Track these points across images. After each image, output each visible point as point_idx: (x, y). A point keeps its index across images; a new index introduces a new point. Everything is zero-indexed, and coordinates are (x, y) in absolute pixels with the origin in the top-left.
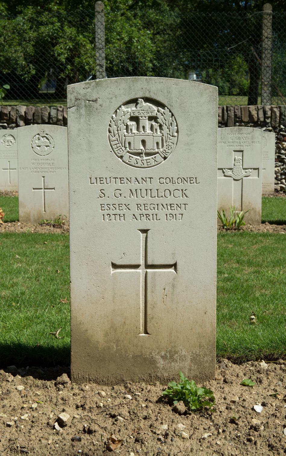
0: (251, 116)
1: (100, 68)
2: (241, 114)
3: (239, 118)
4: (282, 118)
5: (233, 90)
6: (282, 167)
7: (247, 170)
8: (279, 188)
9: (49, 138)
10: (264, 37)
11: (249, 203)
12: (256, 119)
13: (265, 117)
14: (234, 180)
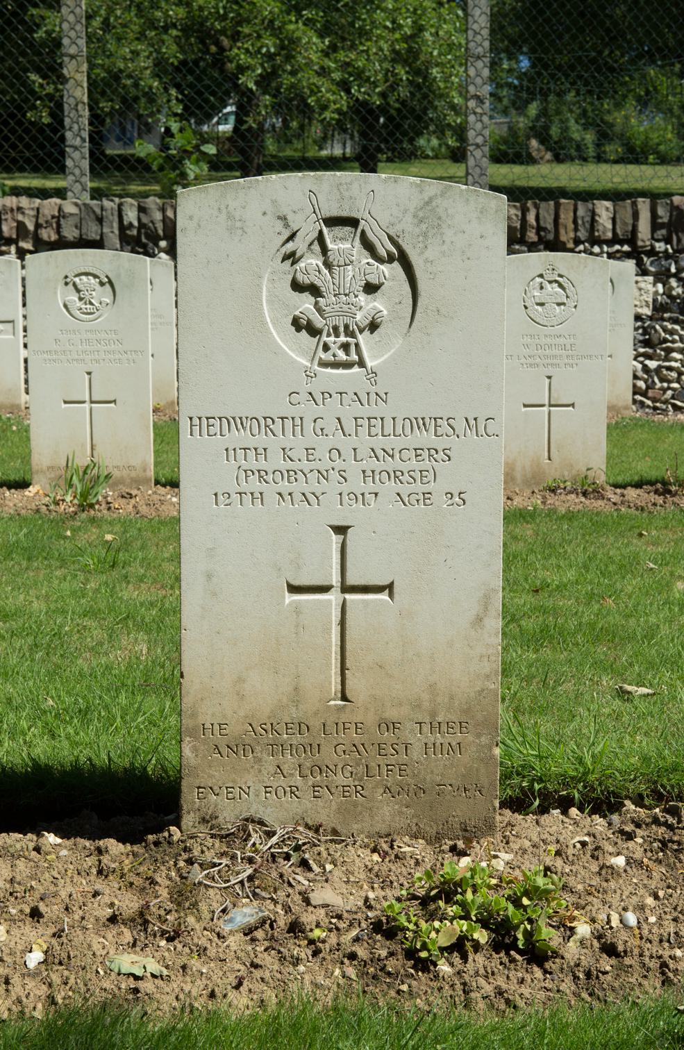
1: (477, 106)
5: (608, 148)
9: (565, 285)
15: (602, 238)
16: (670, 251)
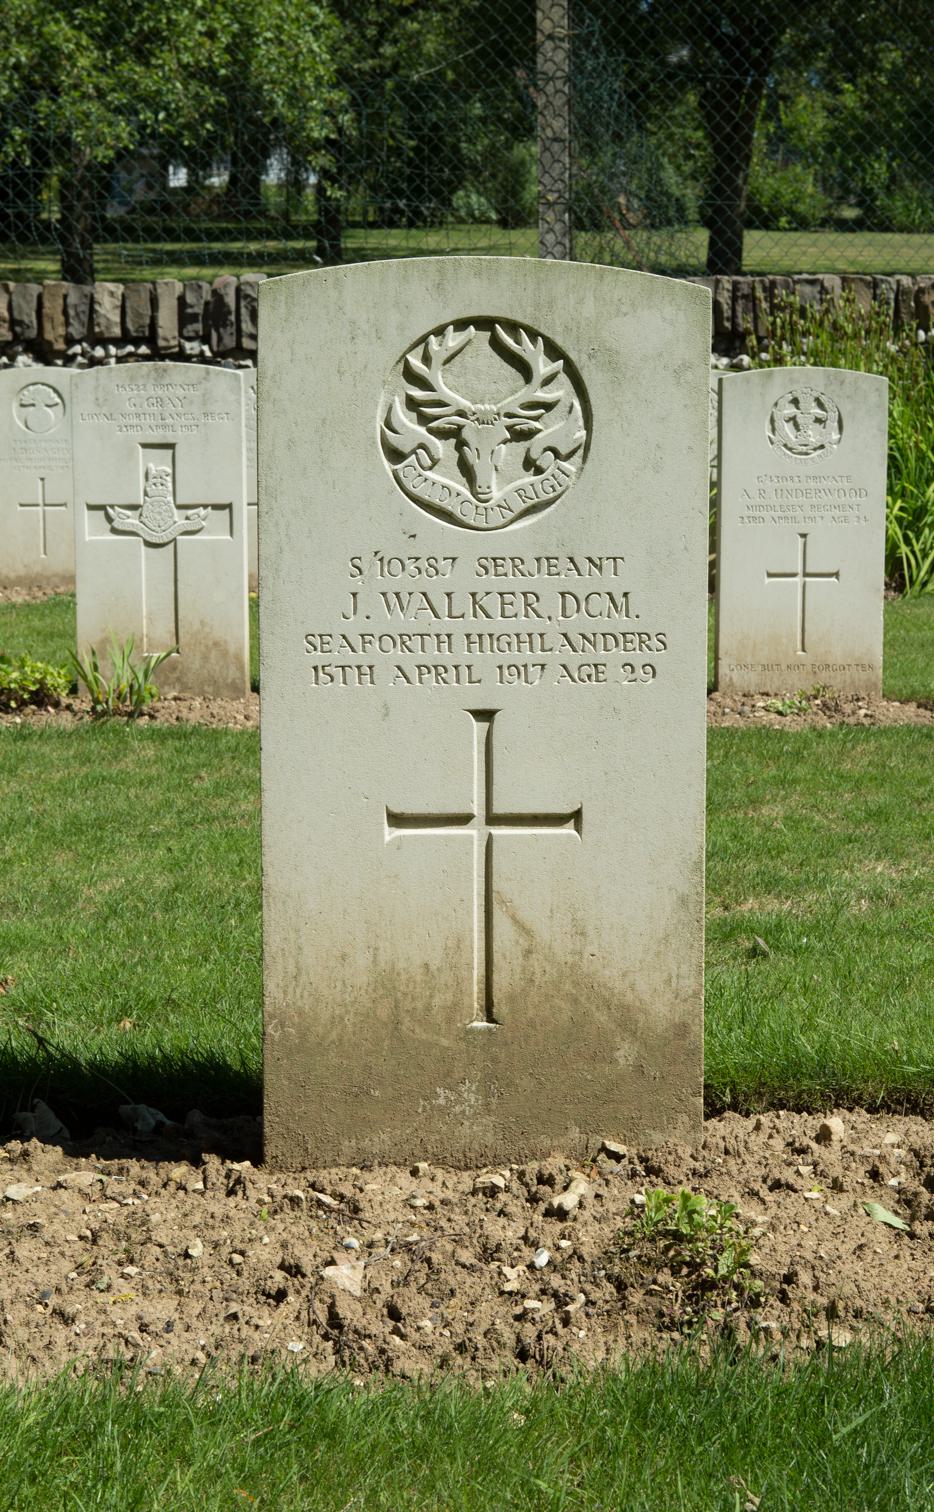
7: (190, 512)
10: (540, 37)
11: (202, 623)
14: (148, 544)
15: (107, 335)
16: (208, 354)
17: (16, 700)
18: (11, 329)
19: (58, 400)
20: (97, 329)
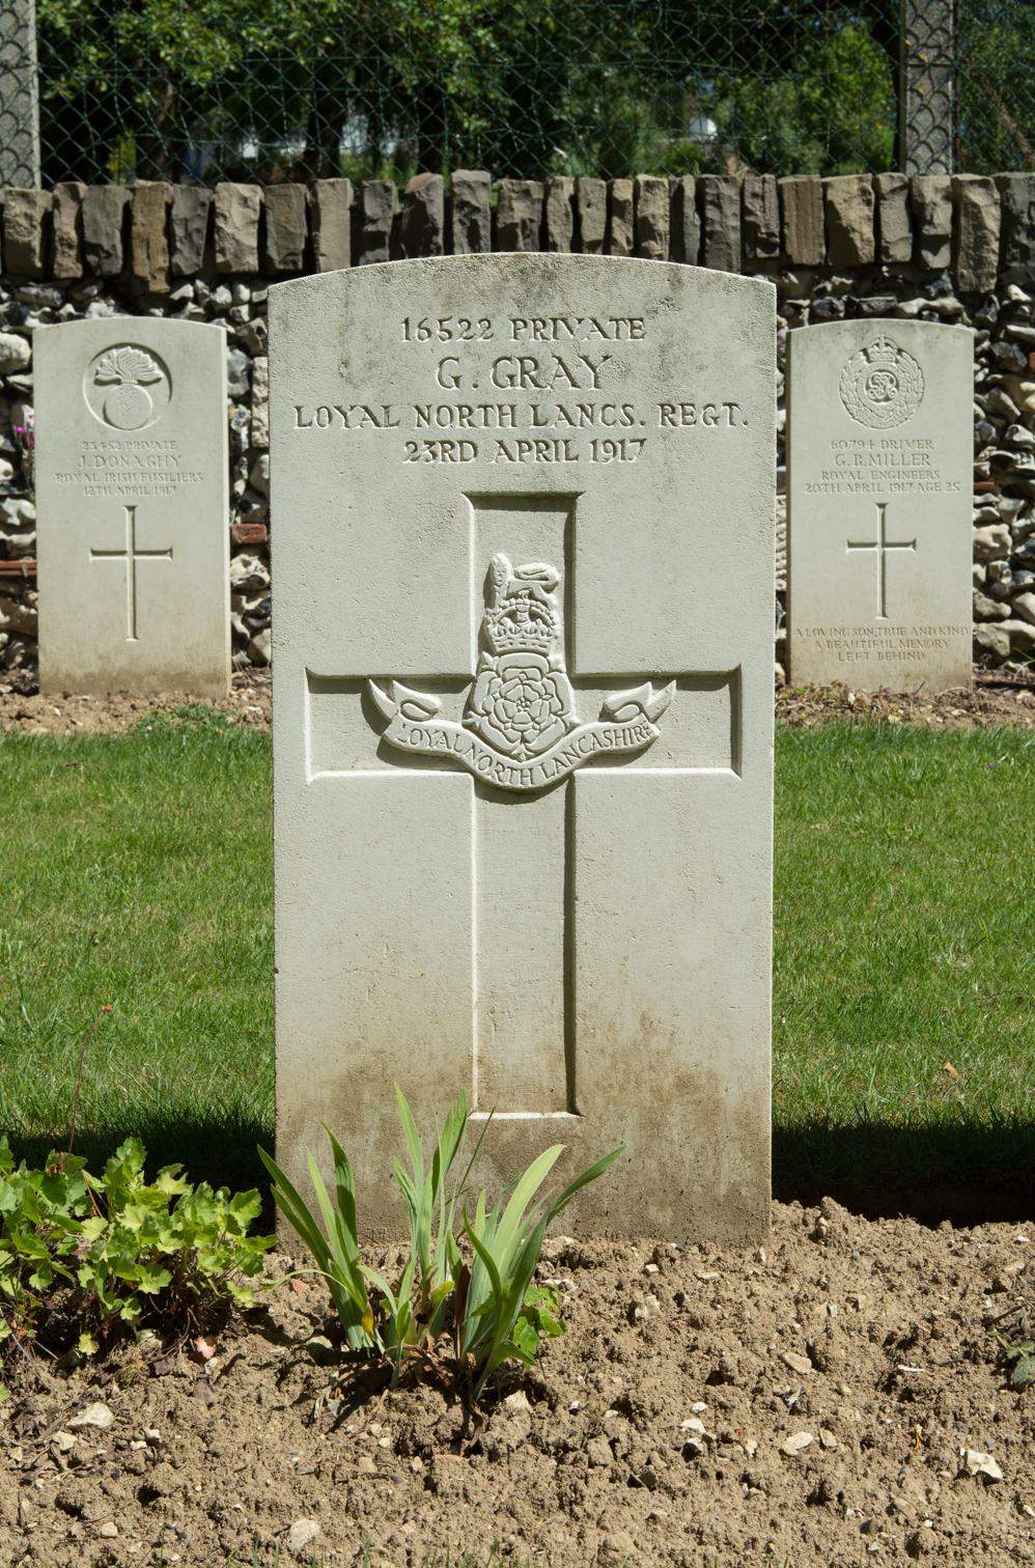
0: (835, 231)
2: (782, 223)
3: (768, 246)
4: (1017, 244)
6: (1019, 523)
7: (615, 697)
8: (1005, 639)
12: (866, 252)
13: (921, 241)
14: (491, 792)
17: (93, 1328)
18: (81, 258)
19: (161, 374)
20: (220, 259)
